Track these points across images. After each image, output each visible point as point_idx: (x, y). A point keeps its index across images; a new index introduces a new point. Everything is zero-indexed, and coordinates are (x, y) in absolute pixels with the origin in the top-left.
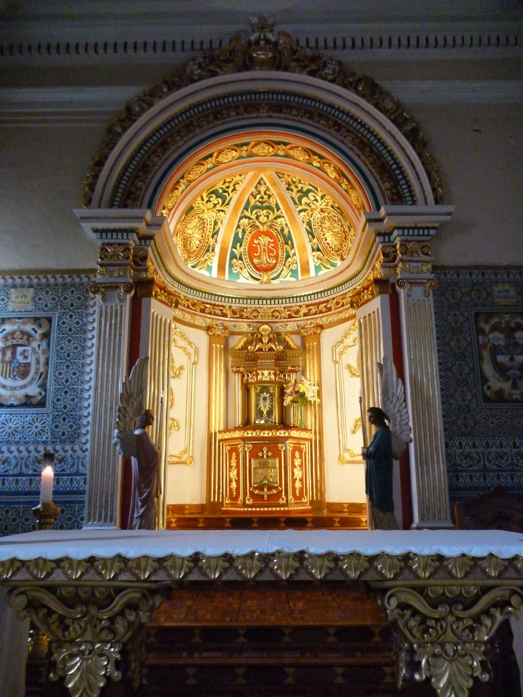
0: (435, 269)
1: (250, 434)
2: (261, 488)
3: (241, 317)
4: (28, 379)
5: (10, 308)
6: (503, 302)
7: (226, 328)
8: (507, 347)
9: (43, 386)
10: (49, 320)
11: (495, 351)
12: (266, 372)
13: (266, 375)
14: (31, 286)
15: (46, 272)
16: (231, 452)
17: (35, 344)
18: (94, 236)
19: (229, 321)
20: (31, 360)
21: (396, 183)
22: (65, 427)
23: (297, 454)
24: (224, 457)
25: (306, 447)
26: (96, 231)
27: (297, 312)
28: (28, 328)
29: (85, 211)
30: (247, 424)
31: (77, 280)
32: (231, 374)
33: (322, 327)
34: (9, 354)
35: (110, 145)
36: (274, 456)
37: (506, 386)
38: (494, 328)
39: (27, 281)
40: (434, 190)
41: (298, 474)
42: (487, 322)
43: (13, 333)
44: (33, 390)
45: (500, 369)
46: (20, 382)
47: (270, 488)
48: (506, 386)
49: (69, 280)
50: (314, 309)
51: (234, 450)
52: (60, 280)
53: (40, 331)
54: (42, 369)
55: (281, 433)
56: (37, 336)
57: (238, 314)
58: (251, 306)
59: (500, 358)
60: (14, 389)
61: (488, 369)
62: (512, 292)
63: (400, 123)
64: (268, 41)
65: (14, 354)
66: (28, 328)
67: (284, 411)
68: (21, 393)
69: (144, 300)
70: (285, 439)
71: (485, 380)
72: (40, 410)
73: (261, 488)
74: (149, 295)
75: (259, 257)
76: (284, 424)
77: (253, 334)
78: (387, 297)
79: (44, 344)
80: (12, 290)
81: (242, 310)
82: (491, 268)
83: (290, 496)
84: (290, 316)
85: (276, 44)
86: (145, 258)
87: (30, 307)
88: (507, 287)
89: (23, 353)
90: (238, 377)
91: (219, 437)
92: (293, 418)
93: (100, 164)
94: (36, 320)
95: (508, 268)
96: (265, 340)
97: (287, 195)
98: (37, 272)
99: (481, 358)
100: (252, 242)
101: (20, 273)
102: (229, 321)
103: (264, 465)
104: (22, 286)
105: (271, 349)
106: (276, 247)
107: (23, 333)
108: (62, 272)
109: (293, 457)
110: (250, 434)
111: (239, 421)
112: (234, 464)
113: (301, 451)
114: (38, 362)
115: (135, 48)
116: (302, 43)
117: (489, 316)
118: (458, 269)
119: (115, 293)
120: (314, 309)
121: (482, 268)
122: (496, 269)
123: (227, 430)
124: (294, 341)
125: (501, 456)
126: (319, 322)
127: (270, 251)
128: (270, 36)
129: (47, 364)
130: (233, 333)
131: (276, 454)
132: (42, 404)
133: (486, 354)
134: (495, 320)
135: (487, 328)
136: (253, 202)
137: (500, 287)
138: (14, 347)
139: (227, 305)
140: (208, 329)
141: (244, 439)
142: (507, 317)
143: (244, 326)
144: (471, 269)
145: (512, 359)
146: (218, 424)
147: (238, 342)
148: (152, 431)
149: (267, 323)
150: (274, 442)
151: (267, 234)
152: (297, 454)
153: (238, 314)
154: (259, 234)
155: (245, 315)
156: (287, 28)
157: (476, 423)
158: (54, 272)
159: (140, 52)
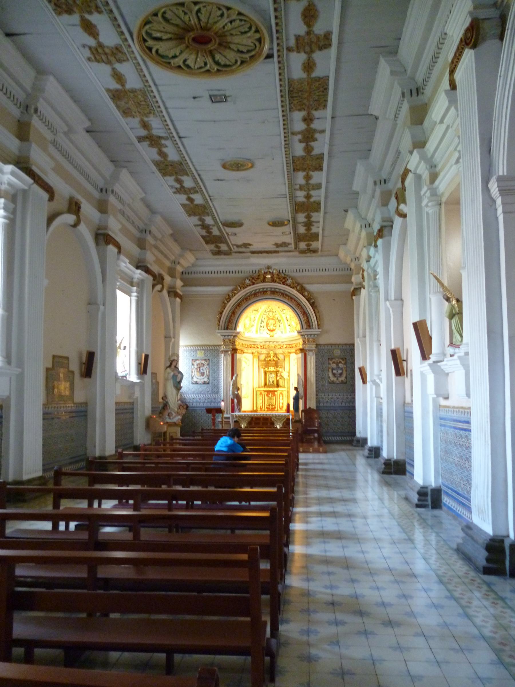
0: (317, 345)
1: (266, 389)
2: (269, 406)
3: (264, 348)
4: (204, 376)
5: (198, 356)
6: (336, 355)
7: (258, 353)
8: (336, 368)
9: (209, 379)
10: (209, 360)
11: (333, 369)
12: (272, 368)
13: (272, 369)
14: (203, 350)
15: (207, 346)
16: (260, 394)
17: (205, 367)
18: (221, 337)
19: (259, 350)
20: (205, 371)
21: (308, 318)
22: (215, 390)
23: (281, 395)
24: (258, 396)
25: (284, 393)
26: (221, 335)
27: (283, 347)
28: (203, 362)
29: (217, 331)
30: (265, 385)
31: (216, 348)
32: (260, 367)
33: (290, 353)
34: (198, 369)
35: (224, 307)
36: (273, 396)
37: (335, 379)
38: (334, 363)
39: (202, 348)
40: (317, 322)
41: (281, 401)
42: (331, 361)
43: (199, 364)
44: (206, 380)
45: (334, 374)
46: (202, 377)
47: (272, 405)
48: (335, 379)
49: (213, 348)
50: (288, 346)
51: (261, 394)
52: (211, 348)
53: (206, 363)
54: (208, 374)
55: (276, 389)
56: (206, 365)
57: (263, 347)
58: (267, 344)
59: (334, 371)
60: (200, 379)
61: (330, 374)
62: (339, 352)
63: (308, 300)
64: (270, 272)
65: (200, 369)
66: (203, 362)
67: (278, 381)
68: (202, 381)
69: (235, 354)
70: (277, 391)
71: (329, 377)
72: (208, 385)
73: (269, 406)
74: (236, 353)
75: (270, 326)
76: (278, 386)
77: (267, 354)
78: (303, 354)
79: (208, 367)
80: (198, 351)
81: (264, 345)
82: (334, 344)
83: (279, 408)
84: (280, 348)
85: (273, 273)
86: (235, 342)
87: (203, 356)
88: (338, 350)
89: (202, 369)
90: (262, 370)
91: (257, 389)
92: (281, 383)
93: (221, 313)
94: (205, 360)
95: (339, 345)
96: (272, 357)
97: (279, 310)
98: (204, 346)
99: (329, 371)
100: (267, 321)
101: (200, 346)
102: (259, 350)
103: (270, 399)
104: (201, 350)
105: (274, 360)
106: (276, 323)
107: (202, 364)
108: (212, 346)
109: (280, 396)
110: (266, 389)
111: (263, 384)
112: (261, 398)
113: (282, 394)
114: (206, 372)
115: (229, 273)
116: (281, 271)
117: (332, 359)
118: (324, 345)
119: (227, 353)
120: (288, 346)
121: (331, 345)
122: (335, 345)
123: (259, 387)
124: (281, 357)
125: (332, 398)
126: (289, 351)
127: (273, 324)
128: (271, 271)
129: (209, 372)
130: (261, 354)
131: (274, 395)
132: (208, 383)
133: (330, 370)
134: (334, 360)
135: (331, 363)
136: (267, 311)
137: (336, 350)
138: (200, 368)
139: (258, 344)
140: (253, 353)
141: (265, 391)
142: (337, 359)
143: (264, 351)
144: (328, 345)
145: (337, 372)
146: (256, 385)
147: (263, 357)
148: (239, 392)
149: (272, 350)
150: (273, 392)
151: (273, 319)
152: (281, 395)
153: (263, 347)
154: (269, 319)
155: (265, 347)
156: (276, 267)
157: (326, 389)
158: (209, 346)
159: (231, 274)
